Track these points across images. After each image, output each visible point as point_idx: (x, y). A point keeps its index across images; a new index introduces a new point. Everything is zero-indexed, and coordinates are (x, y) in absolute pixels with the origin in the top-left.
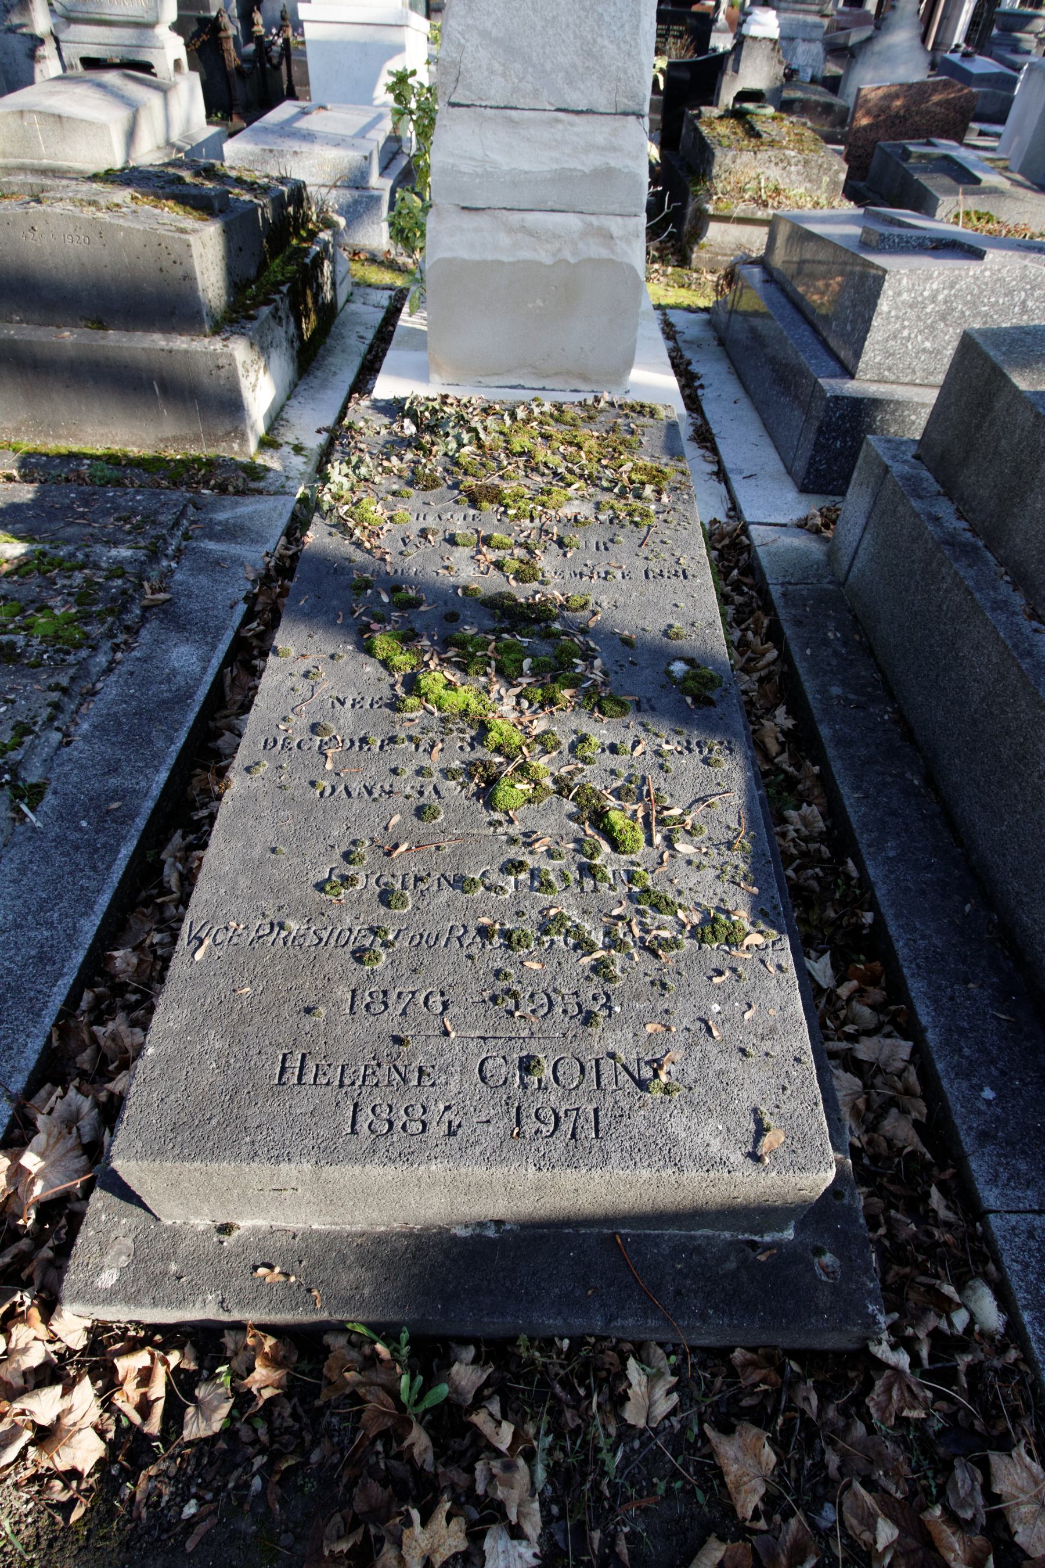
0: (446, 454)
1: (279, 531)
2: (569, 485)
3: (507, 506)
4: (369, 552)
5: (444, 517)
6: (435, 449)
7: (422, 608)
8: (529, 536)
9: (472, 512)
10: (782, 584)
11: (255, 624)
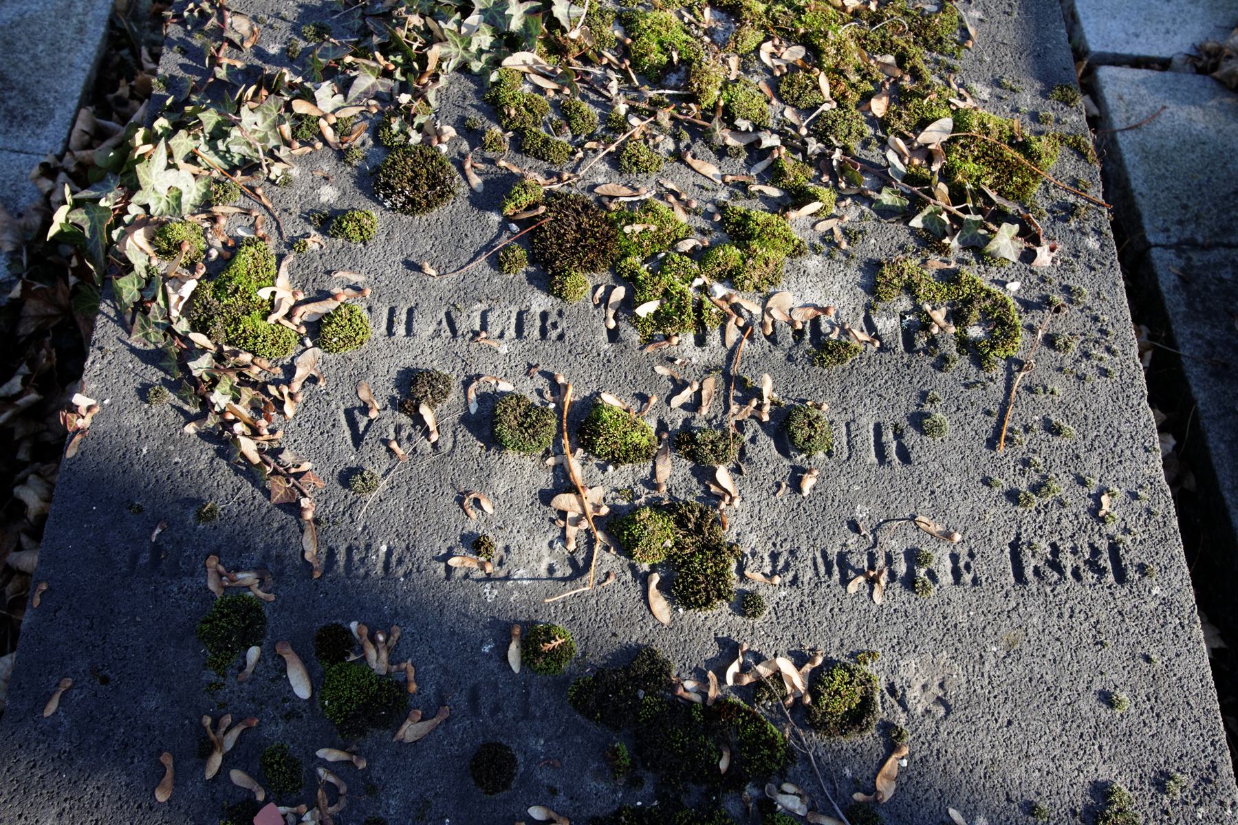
0: (463, 68)
1: (76, 83)
2: (798, 197)
3: (632, 281)
4: (250, 472)
5: (462, 325)
6: (435, 52)
7: (411, 730)
8: (695, 405)
9: (539, 302)
10: (1179, 248)
11: (16, 384)
